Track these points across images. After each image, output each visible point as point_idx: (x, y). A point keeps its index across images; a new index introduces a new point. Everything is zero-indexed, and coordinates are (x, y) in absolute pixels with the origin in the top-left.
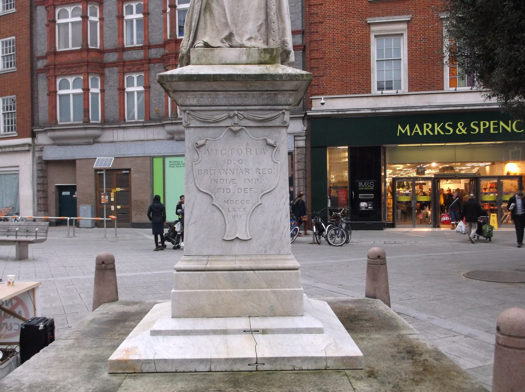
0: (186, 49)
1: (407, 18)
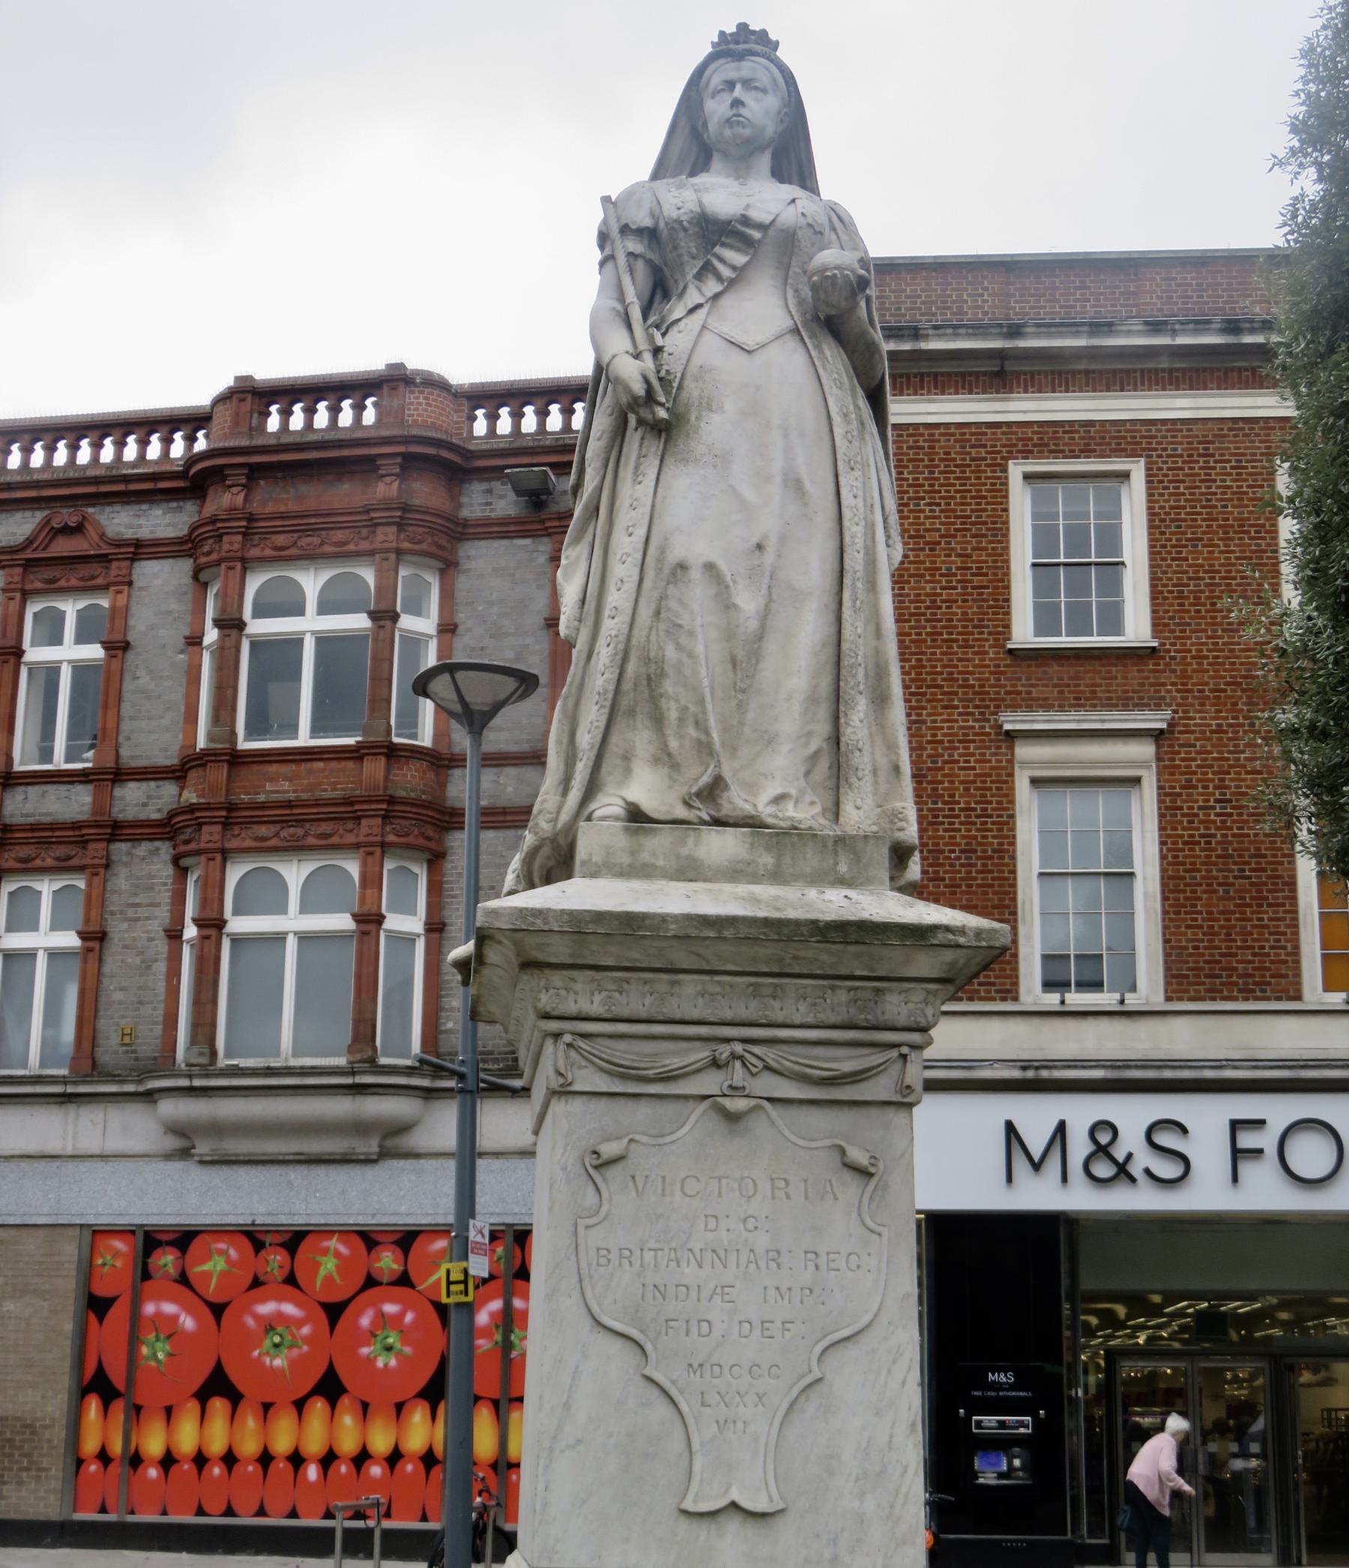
1: (1155, 720)
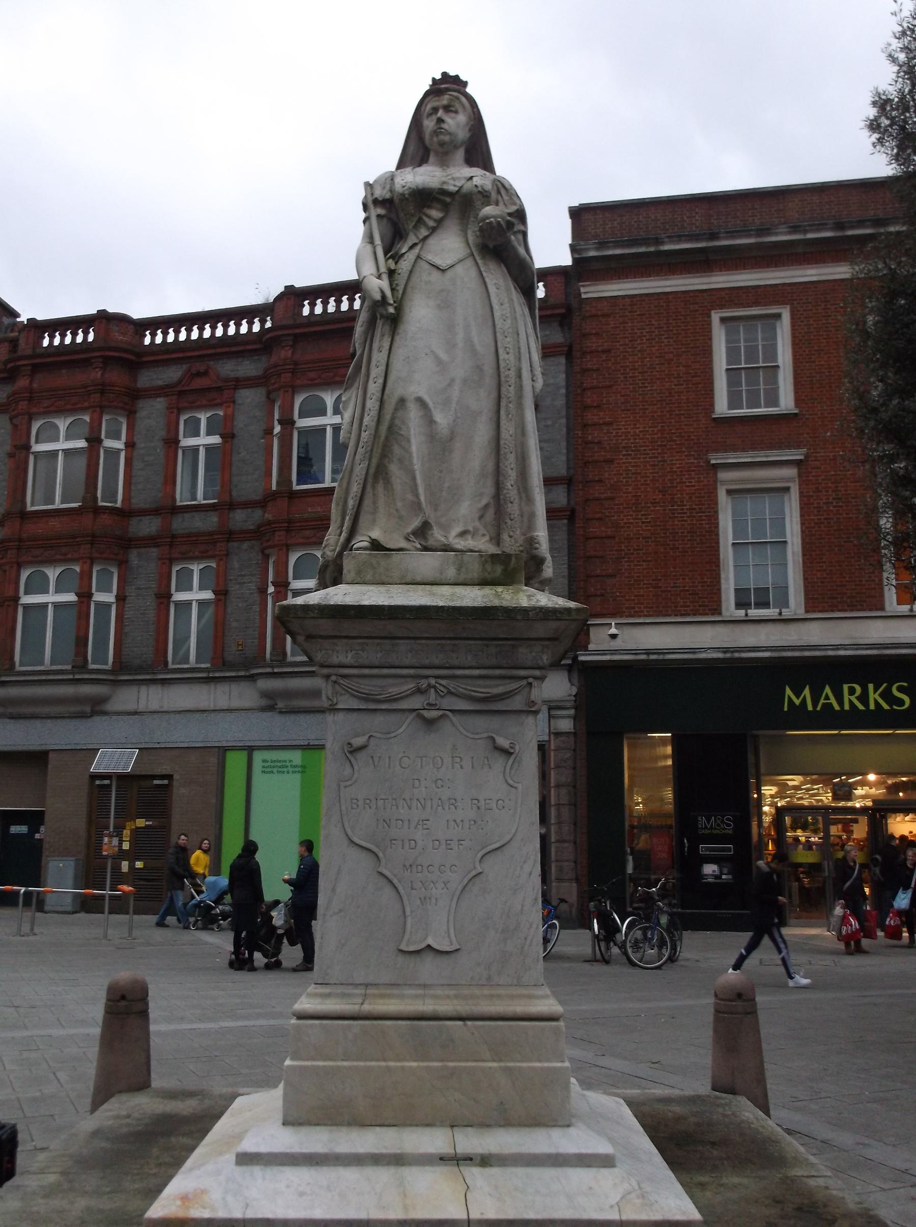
0: (334, 550)
1: (796, 455)
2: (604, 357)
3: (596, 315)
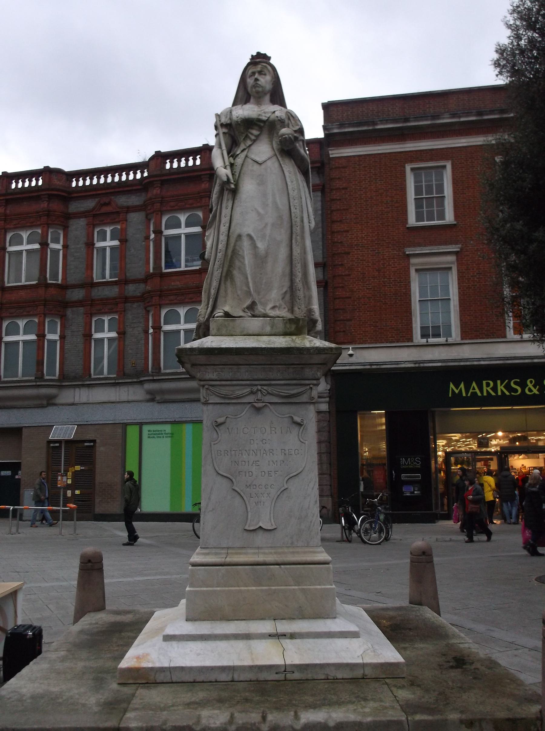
2: (343, 191)
3: (339, 168)
